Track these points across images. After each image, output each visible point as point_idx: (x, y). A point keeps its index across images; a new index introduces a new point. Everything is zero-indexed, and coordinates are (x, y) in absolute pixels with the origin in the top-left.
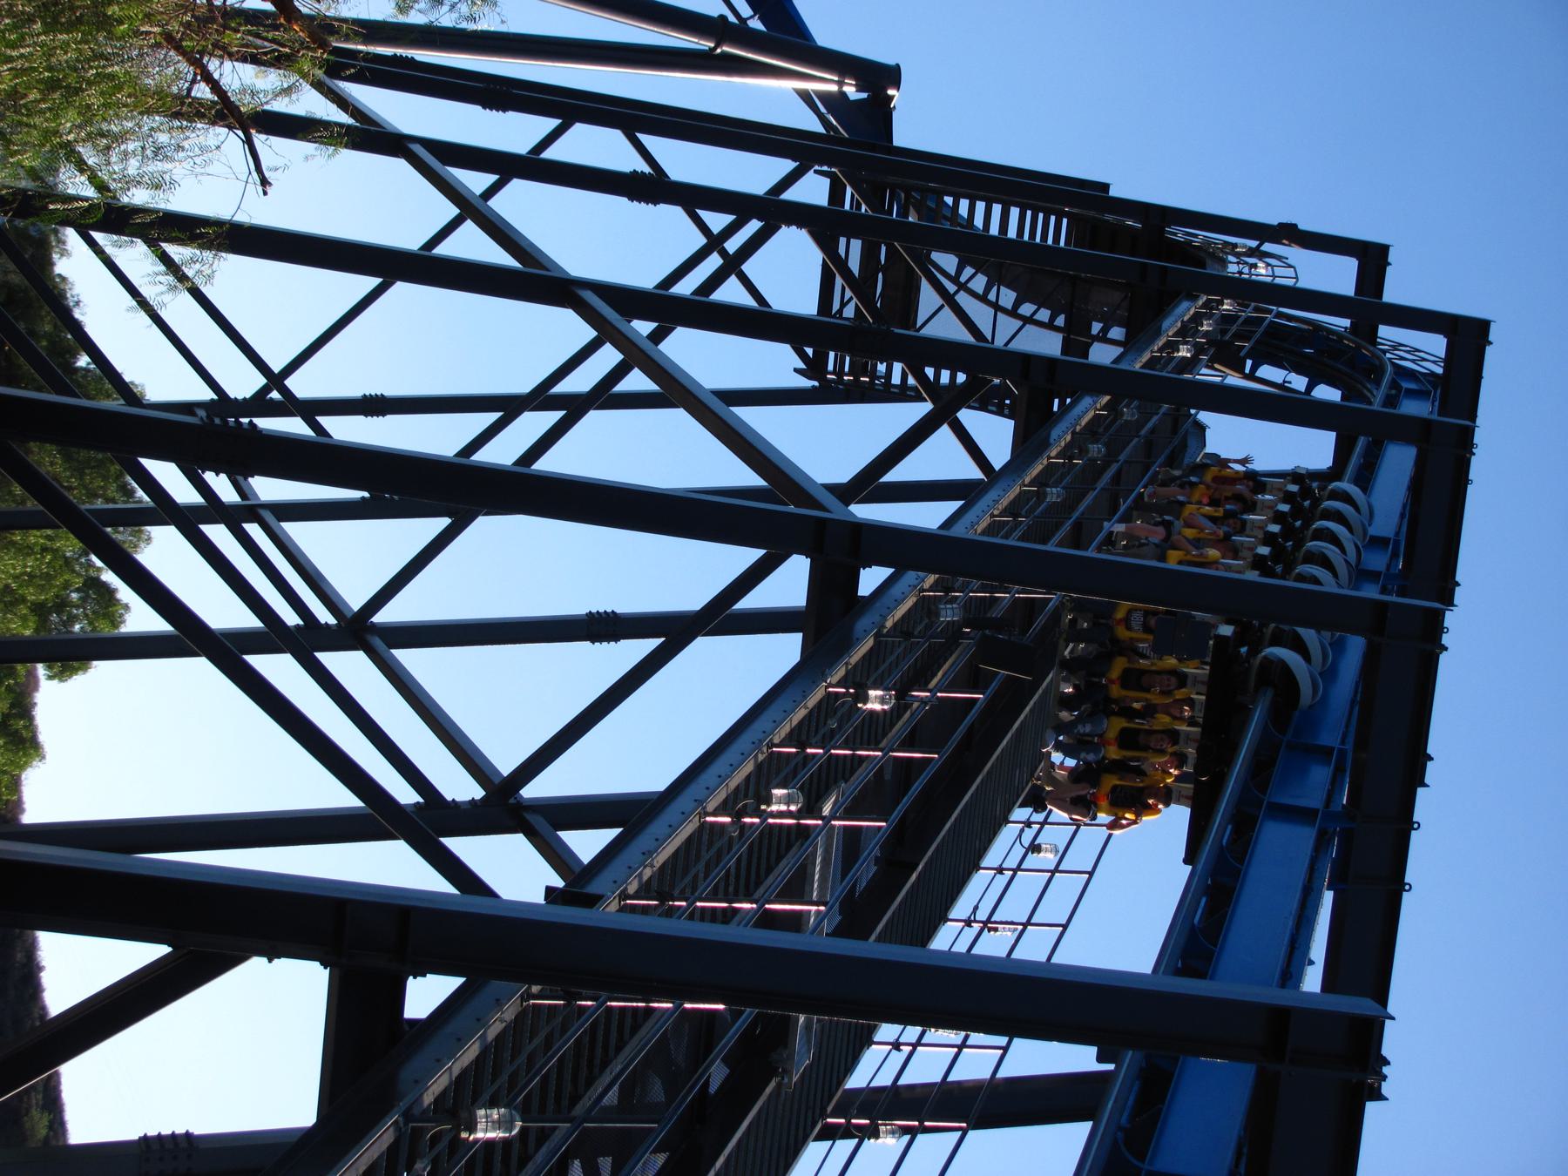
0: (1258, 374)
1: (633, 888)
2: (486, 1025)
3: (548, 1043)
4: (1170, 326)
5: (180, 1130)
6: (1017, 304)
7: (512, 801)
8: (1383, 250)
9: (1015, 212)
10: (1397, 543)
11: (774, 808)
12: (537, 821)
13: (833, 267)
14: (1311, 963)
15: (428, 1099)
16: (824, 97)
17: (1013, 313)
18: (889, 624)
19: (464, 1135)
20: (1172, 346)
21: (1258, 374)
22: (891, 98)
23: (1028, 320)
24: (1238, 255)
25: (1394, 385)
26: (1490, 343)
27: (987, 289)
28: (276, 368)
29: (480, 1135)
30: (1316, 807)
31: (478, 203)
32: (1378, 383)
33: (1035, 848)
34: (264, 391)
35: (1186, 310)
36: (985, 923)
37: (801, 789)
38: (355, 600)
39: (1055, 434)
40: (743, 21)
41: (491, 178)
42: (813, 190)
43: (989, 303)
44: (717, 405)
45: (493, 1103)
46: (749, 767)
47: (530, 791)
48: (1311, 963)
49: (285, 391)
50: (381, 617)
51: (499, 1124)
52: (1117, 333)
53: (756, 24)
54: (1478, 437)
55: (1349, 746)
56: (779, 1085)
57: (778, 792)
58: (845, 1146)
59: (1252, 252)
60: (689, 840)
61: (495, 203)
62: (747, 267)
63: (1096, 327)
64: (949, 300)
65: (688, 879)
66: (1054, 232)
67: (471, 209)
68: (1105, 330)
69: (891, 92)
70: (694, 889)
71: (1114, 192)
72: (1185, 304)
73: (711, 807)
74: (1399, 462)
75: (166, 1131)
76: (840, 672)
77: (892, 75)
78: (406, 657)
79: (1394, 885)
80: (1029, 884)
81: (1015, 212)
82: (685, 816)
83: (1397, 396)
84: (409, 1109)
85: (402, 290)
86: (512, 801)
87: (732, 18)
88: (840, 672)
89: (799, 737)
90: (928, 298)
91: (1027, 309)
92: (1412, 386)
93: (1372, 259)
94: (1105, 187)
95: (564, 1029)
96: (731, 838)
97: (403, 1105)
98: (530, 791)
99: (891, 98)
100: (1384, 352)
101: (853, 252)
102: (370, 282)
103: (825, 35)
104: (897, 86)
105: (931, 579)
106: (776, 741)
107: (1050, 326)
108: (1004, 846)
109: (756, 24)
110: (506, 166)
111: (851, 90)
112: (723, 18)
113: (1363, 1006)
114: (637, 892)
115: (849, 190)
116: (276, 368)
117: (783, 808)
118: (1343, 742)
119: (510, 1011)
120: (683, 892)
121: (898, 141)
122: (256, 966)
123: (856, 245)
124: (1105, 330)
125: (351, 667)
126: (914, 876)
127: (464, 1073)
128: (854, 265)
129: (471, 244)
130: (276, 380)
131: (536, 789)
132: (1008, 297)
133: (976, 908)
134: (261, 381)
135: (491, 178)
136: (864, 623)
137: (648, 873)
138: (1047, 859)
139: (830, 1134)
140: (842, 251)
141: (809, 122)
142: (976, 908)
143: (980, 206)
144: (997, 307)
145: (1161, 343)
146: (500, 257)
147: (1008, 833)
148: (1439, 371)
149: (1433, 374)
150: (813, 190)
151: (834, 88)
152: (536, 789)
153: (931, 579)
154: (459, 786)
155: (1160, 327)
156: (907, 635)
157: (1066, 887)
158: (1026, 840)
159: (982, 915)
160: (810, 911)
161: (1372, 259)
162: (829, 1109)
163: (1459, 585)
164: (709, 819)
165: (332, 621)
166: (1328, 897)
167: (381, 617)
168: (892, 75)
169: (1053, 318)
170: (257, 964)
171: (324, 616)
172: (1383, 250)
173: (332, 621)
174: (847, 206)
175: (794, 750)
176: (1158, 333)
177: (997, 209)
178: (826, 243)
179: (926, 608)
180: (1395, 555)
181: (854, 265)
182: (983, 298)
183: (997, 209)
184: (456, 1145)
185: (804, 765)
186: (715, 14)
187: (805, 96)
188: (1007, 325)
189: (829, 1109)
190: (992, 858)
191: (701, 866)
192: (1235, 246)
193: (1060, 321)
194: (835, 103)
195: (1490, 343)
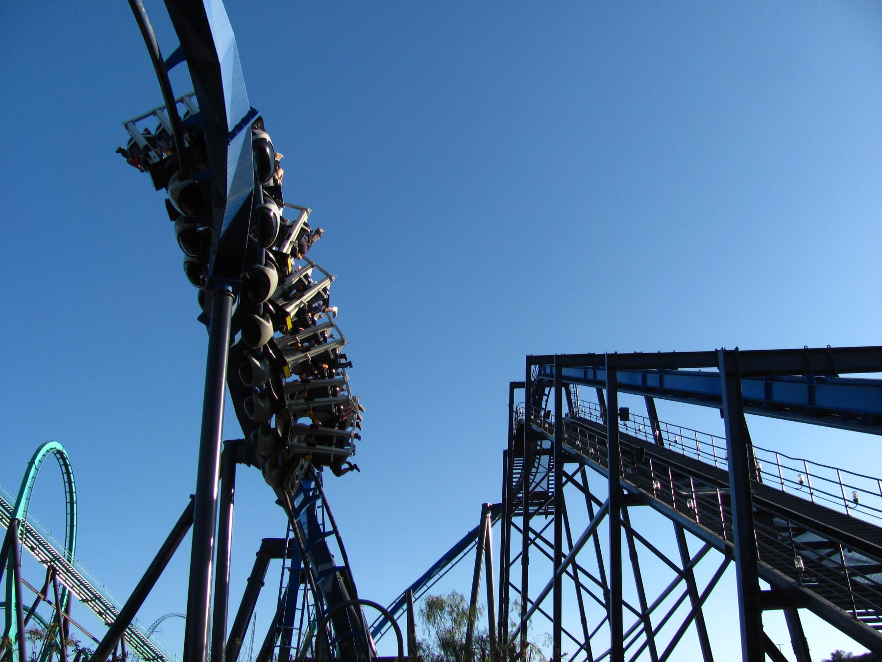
0: (544, 408)
1: (721, 538)
2: (769, 569)
3: (771, 552)
4: (539, 430)
5: (791, 644)
6: (535, 467)
7: (685, 572)
8: (511, 383)
9: (514, 471)
10: (585, 368)
11: (693, 506)
12: (689, 565)
13: (537, 513)
14: (700, 370)
15: (793, 580)
16: (492, 521)
17: (537, 468)
18: (634, 485)
19: (803, 570)
20: (545, 429)
21: (544, 408)
22: (490, 505)
23: (539, 464)
24: (518, 418)
25: (544, 375)
26: (616, 352)
27: (533, 475)
28: (579, 647)
29: (802, 566)
30: (641, 376)
31: (535, 605)
32: (543, 379)
33: (676, 442)
34: (585, 649)
35: (534, 427)
36: (698, 451)
37: (686, 500)
38: (637, 618)
39: (573, 453)
40: (476, 543)
41: (528, 603)
42: (518, 521)
43: (536, 474)
44: (594, 520)
45: (794, 564)
46: (681, 514)
47: (681, 567)
48: (700, 370)
49: (584, 644)
50: (640, 611)
51: (799, 561)
52: (539, 443)
53: (477, 540)
54: (559, 353)
55: (641, 370)
56: (755, 494)
57: (688, 505)
58: (762, 475)
59: (517, 412)
60: (704, 525)
61: (534, 600)
62: (538, 532)
63: (538, 448)
64: (538, 484)
65: (716, 524)
66: (519, 462)
67: (536, 606)
68: (539, 445)
69: (489, 506)
70: (719, 522)
71: (506, 448)
72: (533, 427)
73: (695, 522)
74: (566, 371)
75: (792, 647)
76: (650, 495)
77: (485, 506)
78: (649, 604)
79: (829, 352)
80: (685, 442)
81: (514, 471)
82: (698, 527)
83: (546, 374)
84: (797, 585)
85: (564, 625)
86: (685, 572)
87: (477, 546)
88: (650, 495)
89: (670, 502)
90: (538, 489)
91: (536, 465)
92: (543, 371)
93: (514, 386)
94: (505, 451)
95: (765, 549)
96: (702, 515)
97: (797, 587)
98: (681, 567)
99: (490, 505)
100: (535, 379)
101: (532, 509)
102: (552, 616)
103: (477, 523)
104: (487, 504)
105: (621, 477)
106: (672, 508)
107: (539, 459)
108: (677, 449)
109: (477, 540)
110: (525, 598)
111: (489, 515)
112: (476, 548)
113: (721, 357)
114: (722, 536)
115: (516, 512)
116: (579, 647)
117: (692, 503)
118: (640, 372)
119: (764, 563)
120: (720, 525)
121: (500, 501)
122: (766, 630)
123: (530, 508)
124: (539, 445)
125: (655, 619)
126: (692, 470)
127: (783, 572)
128: (536, 508)
129: (548, 605)
130: (582, 647)
131: (680, 566)
132: (534, 470)
133: (695, 454)
134: (583, 650)
135: (528, 603)
136: (634, 491)
137: (716, 534)
138: (678, 438)
139: (760, 479)
140: (533, 511)
141: (499, 523)
142: (695, 454)
143: (514, 480)
144: (537, 472)
145: (544, 431)
146: (551, 594)
147: (673, 449)
148: (538, 366)
149: (539, 367)
150: (518, 521)
151: (490, 519)
152: (681, 566)
153: (621, 477)
154: (683, 586)
155: (540, 433)
156: (637, 480)
157: (684, 433)
158: (674, 444)
159: (696, 452)
160: (720, 493)
161: (514, 386)
162: (755, 481)
163: (716, 349)
164: (698, 521)
165: (643, 624)
166: (680, 369)
167: (640, 611)
168: (485, 506)
169: (537, 458)
170: (765, 630)
171: (642, 626)
172: (511, 383)
173: (643, 624)
174: (522, 512)
175: (674, 504)
176: (542, 432)
177: (514, 476)
178: (532, 515)
179: (628, 477)
180: (588, 368)
181: (536, 508)
182: (535, 476)
183: (514, 476)
184: (806, 571)
185: (678, 500)
186: (476, 550)
187: (492, 525)
188: (541, 469)
189: (755, 481)
190: (681, 452)
191: (712, 521)
192: (515, 418)
193: (538, 457)
194: (493, 518)
195: (616, 352)
